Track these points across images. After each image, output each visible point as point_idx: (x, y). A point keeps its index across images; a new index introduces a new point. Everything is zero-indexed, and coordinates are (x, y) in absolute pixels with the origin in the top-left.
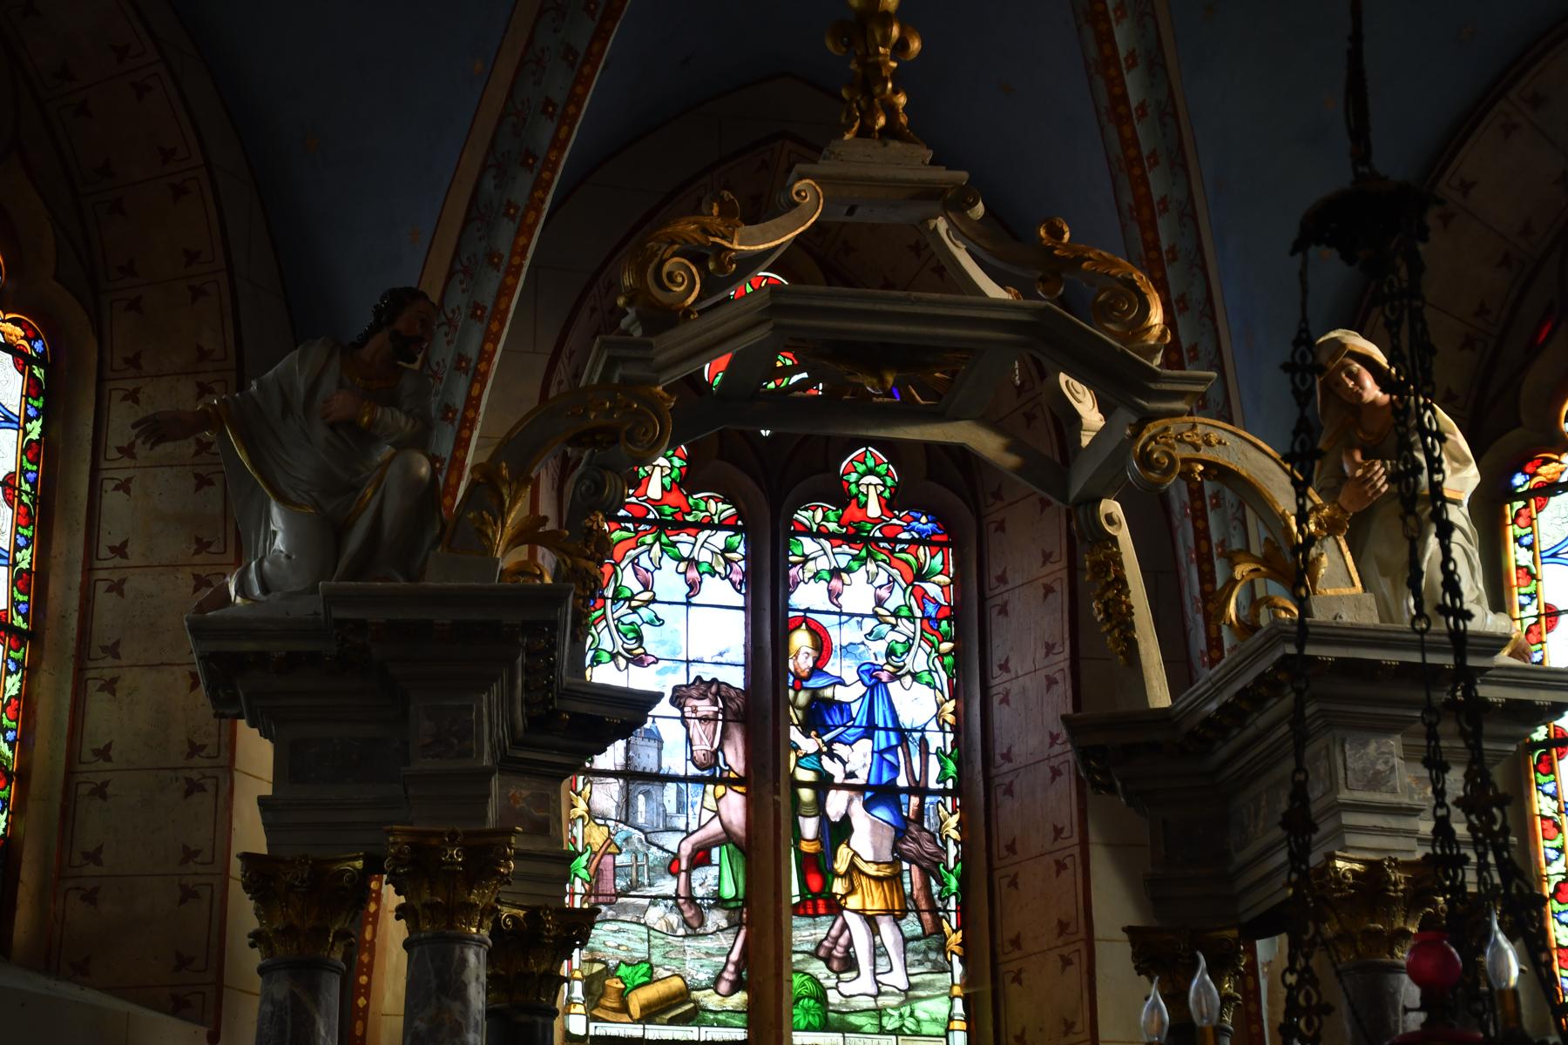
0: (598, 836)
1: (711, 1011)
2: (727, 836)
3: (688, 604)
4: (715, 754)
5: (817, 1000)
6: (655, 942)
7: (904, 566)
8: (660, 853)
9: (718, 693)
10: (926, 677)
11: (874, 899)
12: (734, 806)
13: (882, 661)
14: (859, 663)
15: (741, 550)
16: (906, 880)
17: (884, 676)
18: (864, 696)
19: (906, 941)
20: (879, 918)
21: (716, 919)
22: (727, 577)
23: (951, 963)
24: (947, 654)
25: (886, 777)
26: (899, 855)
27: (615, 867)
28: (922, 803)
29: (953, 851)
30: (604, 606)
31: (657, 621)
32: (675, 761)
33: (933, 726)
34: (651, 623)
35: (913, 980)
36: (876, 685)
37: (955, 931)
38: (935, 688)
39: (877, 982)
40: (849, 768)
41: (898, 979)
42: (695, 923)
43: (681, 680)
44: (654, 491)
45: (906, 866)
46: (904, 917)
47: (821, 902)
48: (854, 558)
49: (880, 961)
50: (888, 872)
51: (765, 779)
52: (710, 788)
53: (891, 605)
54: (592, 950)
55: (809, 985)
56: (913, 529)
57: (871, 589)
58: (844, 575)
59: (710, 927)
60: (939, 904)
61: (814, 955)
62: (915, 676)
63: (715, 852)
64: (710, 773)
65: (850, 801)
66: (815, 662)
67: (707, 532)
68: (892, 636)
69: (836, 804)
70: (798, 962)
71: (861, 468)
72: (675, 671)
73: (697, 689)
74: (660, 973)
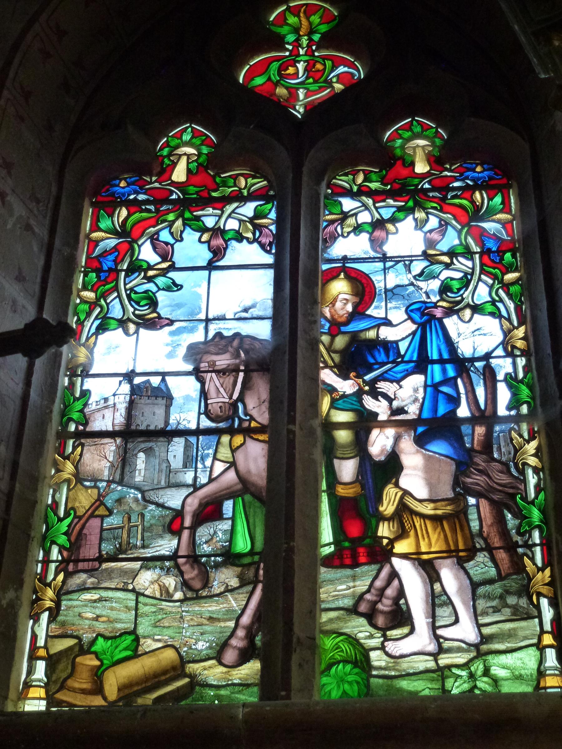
0: (84, 500)
1: (211, 686)
2: (244, 488)
3: (211, 266)
4: (234, 406)
5: (355, 664)
6: (143, 609)
7: (459, 211)
8: (158, 512)
9: (240, 346)
10: (489, 308)
11: (432, 542)
12: (255, 456)
13: (434, 298)
14: (407, 303)
15: (273, 215)
16: (473, 516)
17: (438, 313)
18: (414, 333)
19: (475, 586)
20: (437, 563)
21: (226, 577)
22: (255, 240)
23: (538, 607)
24: (513, 284)
25: (442, 410)
26: (460, 489)
27: (102, 530)
28: (489, 434)
29: (532, 480)
30: (117, 279)
31: (175, 286)
32: (186, 415)
33: (500, 352)
34: (168, 289)
35: (486, 631)
36: (429, 321)
37: (542, 569)
38: (500, 317)
39: (437, 638)
40: (395, 404)
41: (465, 630)
42: (197, 584)
43: (198, 336)
44: (179, 174)
45: (472, 501)
46: (471, 558)
47: (361, 550)
48: (399, 209)
49: (439, 612)
50: (449, 509)
51: (294, 434)
52: (225, 439)
53: (444, 246)
54: (63, 624)
55: (345, 647)
56: (467, 178)
57: (420, 235)
58: (390, 226)
59: (217, 588)
60: (519, 539)
61: (353, 611)
62: (476, 309)
63: (228, 507)
64: (227, 423)
65: (397, 439)
66: (355, 307)
67: (235, 205)
68: (446, 274)
69: (380, 442)
70: (331, 620)
71: (407, 134)
72: (192, 330)
73: (216, 345)
74: (148, 645)
